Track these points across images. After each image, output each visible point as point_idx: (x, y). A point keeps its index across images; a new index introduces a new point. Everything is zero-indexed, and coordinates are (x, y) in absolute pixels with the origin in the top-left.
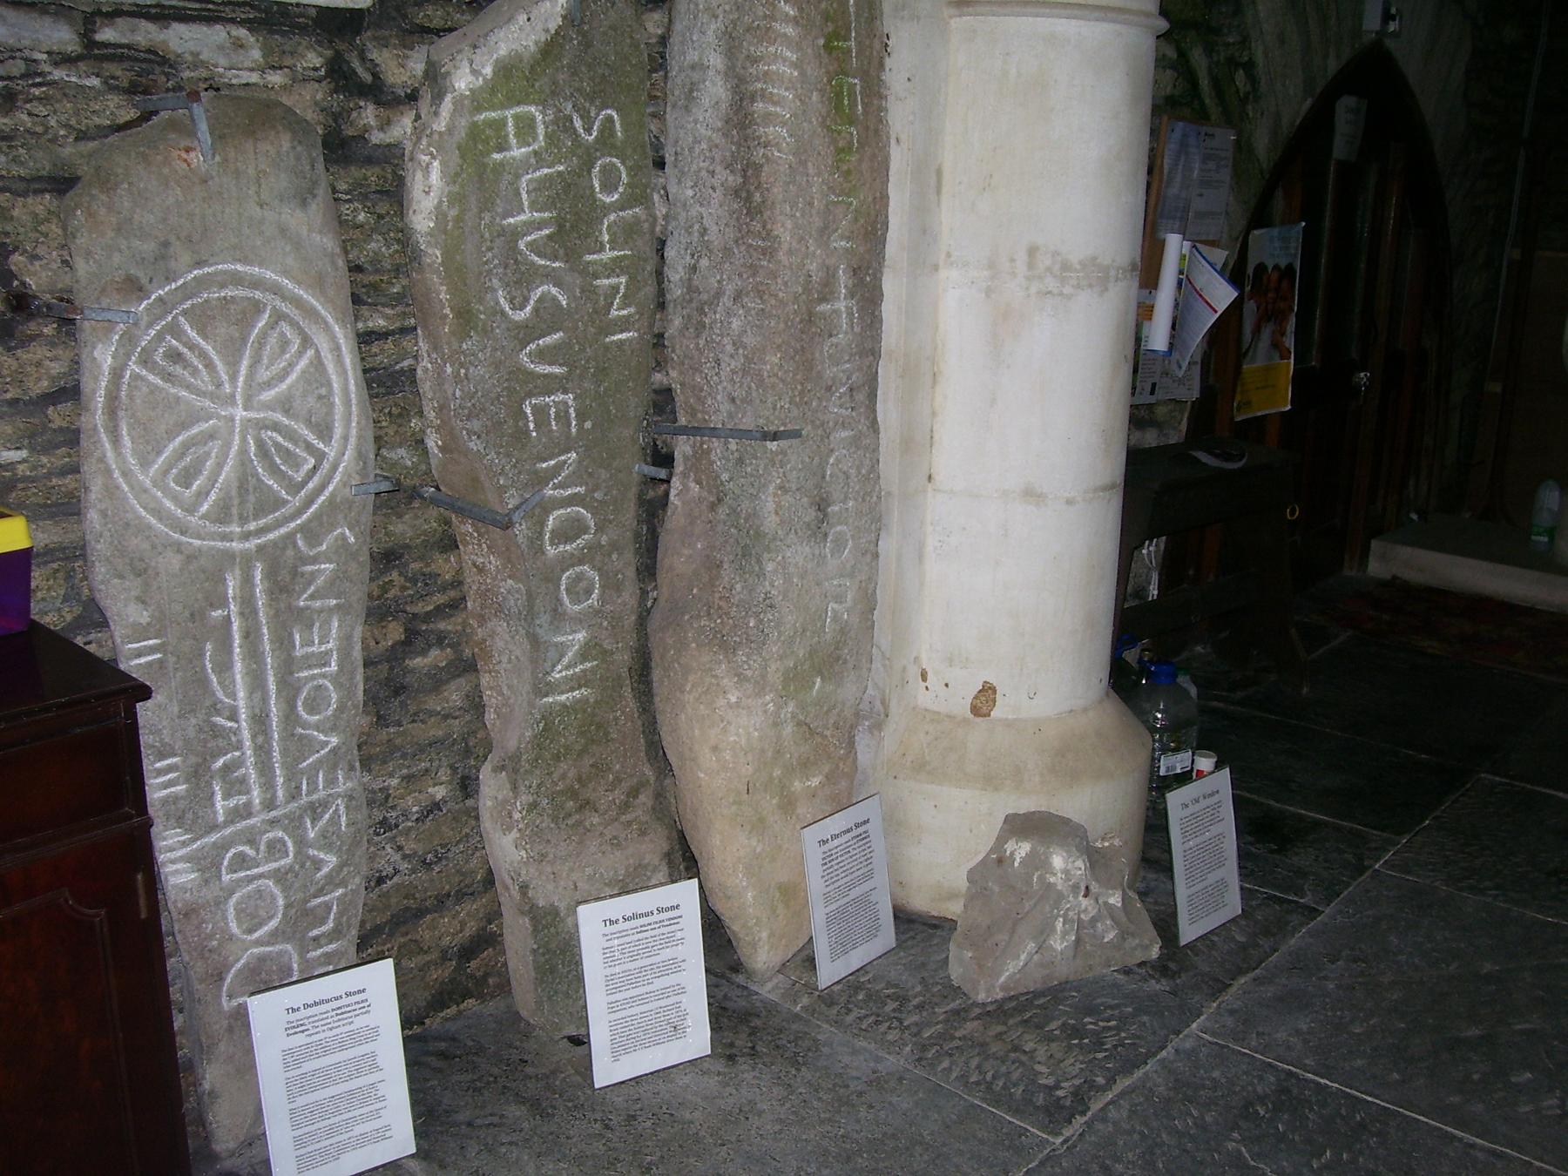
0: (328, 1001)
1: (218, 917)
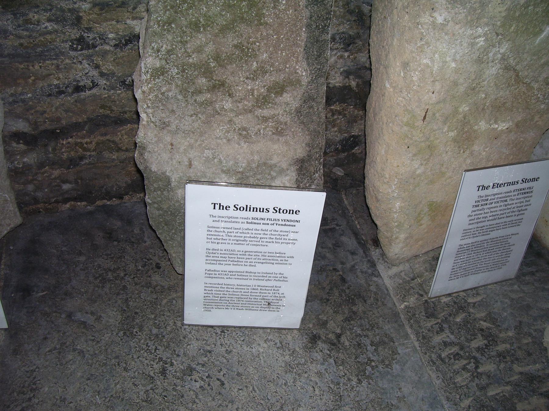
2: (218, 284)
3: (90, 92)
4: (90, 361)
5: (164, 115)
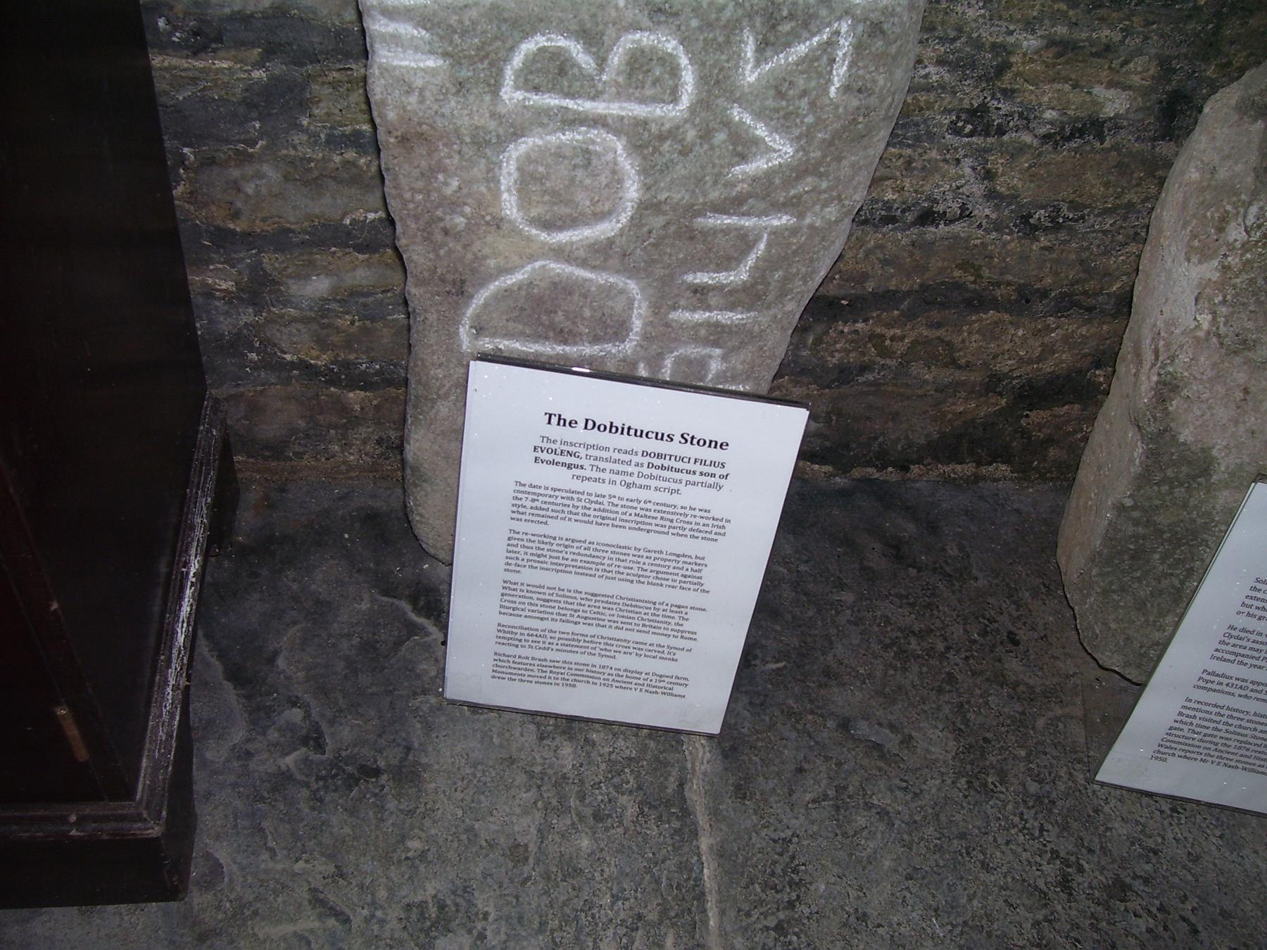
0: (640, 434)
1: (479, 171)
2: (1216, 706)
3: (947, 229)
4: (905, 836)
5: (1250, 325)
